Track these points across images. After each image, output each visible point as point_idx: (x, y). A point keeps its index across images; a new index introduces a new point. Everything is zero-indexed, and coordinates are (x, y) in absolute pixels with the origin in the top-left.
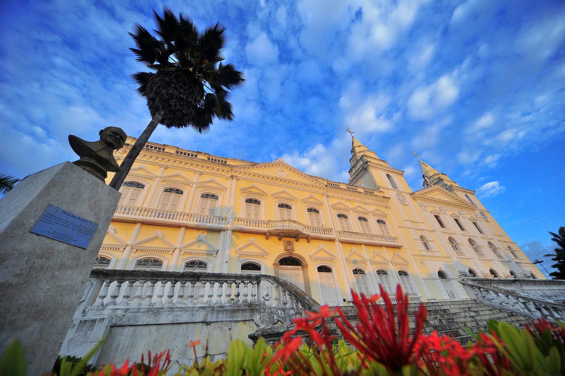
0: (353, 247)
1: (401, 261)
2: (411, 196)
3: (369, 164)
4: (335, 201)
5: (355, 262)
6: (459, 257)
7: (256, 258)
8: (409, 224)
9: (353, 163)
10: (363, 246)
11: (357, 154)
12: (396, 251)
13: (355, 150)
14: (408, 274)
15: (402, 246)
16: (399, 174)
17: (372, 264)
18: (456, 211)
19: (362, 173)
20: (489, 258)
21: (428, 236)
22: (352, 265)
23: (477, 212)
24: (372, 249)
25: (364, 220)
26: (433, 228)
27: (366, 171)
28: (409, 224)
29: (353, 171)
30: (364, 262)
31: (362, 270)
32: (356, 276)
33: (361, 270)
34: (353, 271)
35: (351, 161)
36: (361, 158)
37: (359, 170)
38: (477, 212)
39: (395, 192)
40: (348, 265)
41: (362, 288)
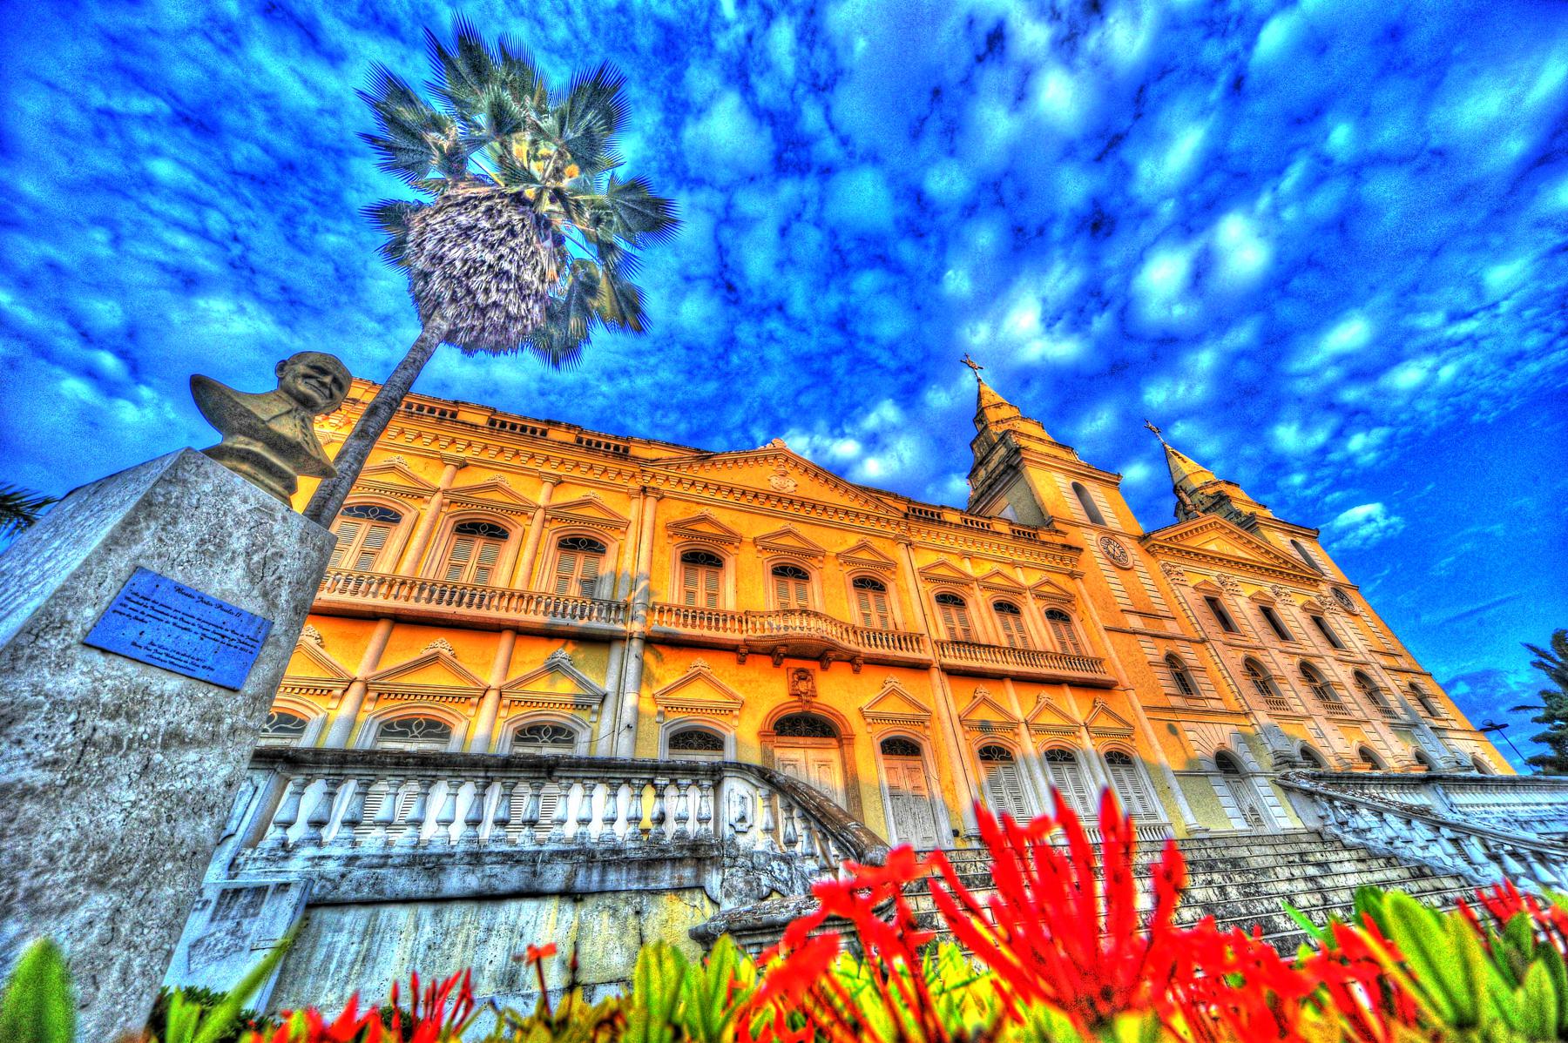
1: (1112, 724)
4: (932, 558)
5: (985, 727)
6: (1273, 712)
8: (1135, 622)
12: (1101, 697)
13: (984, 415)
22: (977, 735)
28: (1135, 622)
38: (1325, 589)
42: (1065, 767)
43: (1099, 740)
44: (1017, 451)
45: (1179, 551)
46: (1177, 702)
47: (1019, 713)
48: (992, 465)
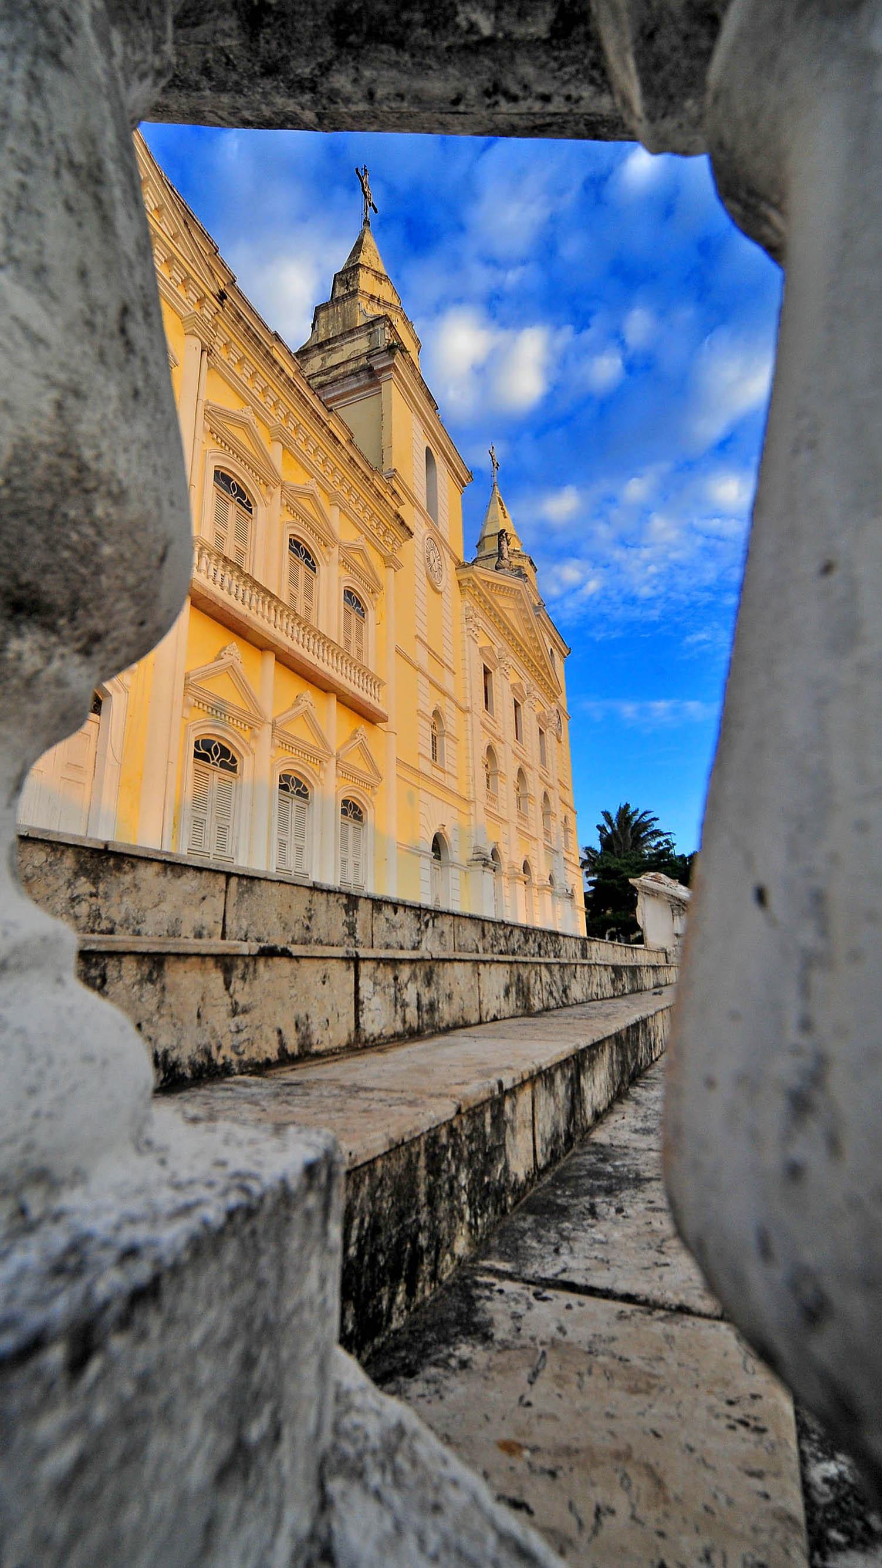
0: (234, 644)
1: (361, 765)
2: (459, 571)
3: (398, 360)
4: (231, 404)
5: (217, 709)
6: (488, 808)
7: (238, 730)
8: (421, 657)
9: (328, 331)
10: (270, 659)
11: (360, 300)
12: (363, 727)
13: (355, 277)
14: (364, 819)
15: (385, 720)
16: (457, 475)
17: (277, 742)
18: (527, 681)
19: (349, 388)
20: (532, 832)
21: (452, 720)
22: (200, 716)
23: (554, 706)
24: (294, 687)
25: (306, 562)
26: (469, 701)
27: (370, 386)
28: (421, 657)
29: (311, 362)
30: (252, 722)
31: (232, 752)
32: (199, 768)
33: (225, 752)
34: (197, 744)
35: (322, 315)
36: (372, 324)
37: (341, 370)
38: (554, 706)
39: (426, 528)
40: (187, 714)
41: (208, 824)
42: (296, 802)
43: (345, 782)
44: (394, 348)
45: (486, 601)
46: (425, 767)
47: (270, 709)
48: (335, 359)
